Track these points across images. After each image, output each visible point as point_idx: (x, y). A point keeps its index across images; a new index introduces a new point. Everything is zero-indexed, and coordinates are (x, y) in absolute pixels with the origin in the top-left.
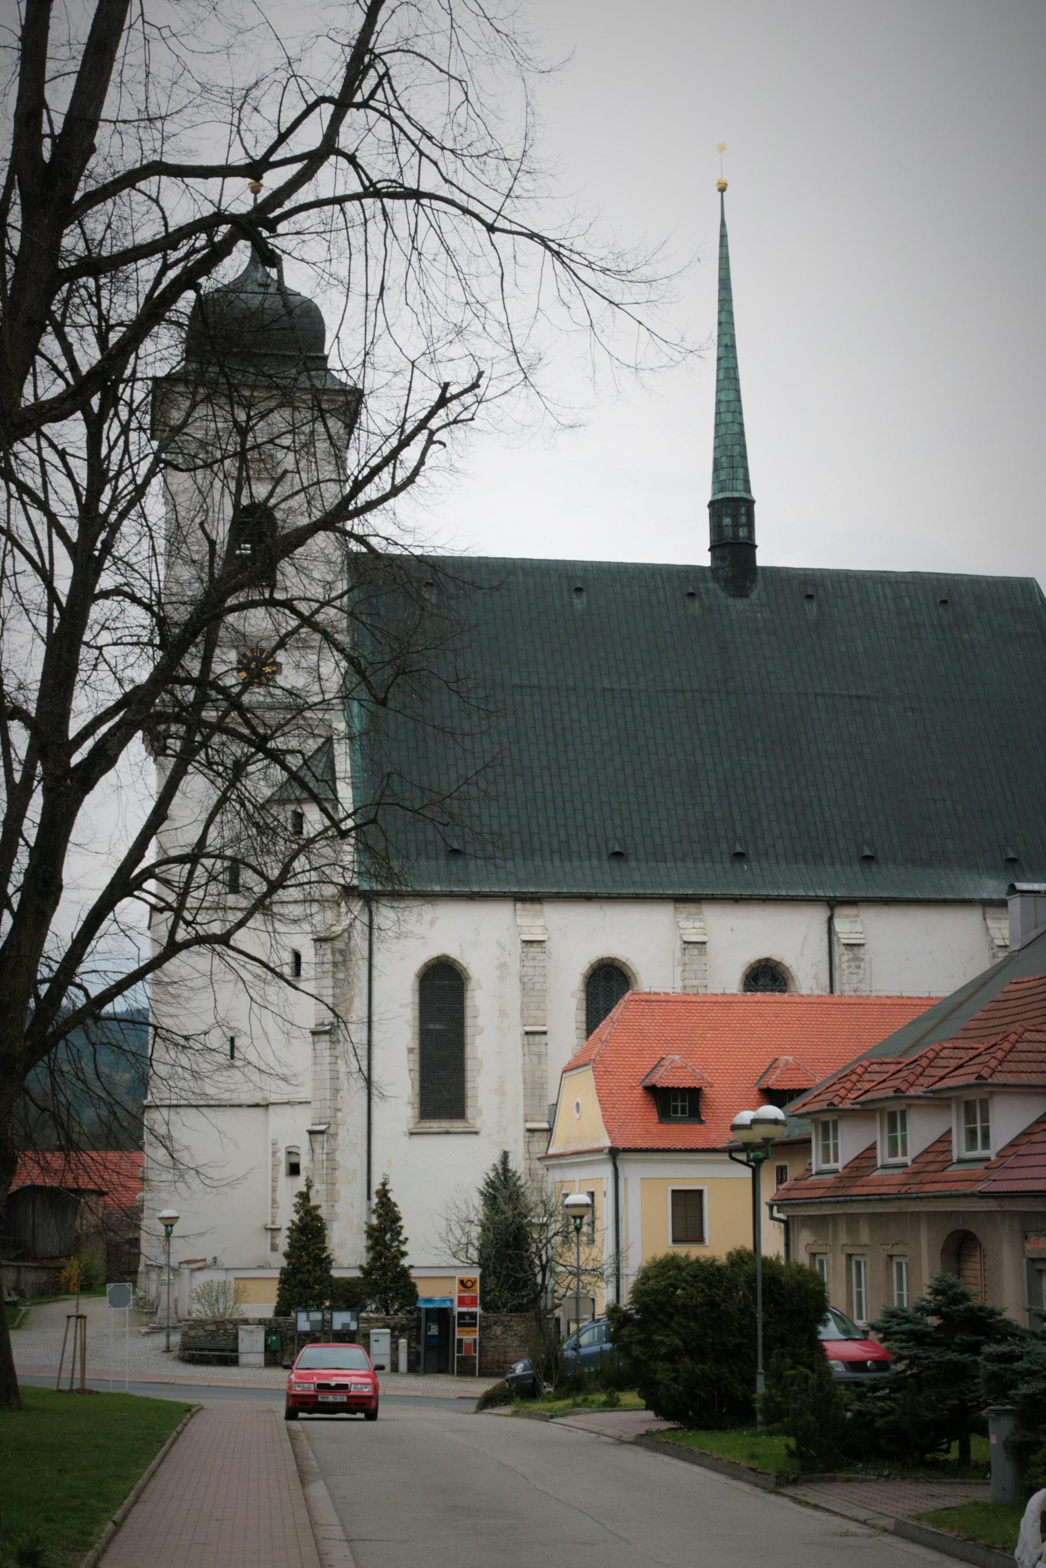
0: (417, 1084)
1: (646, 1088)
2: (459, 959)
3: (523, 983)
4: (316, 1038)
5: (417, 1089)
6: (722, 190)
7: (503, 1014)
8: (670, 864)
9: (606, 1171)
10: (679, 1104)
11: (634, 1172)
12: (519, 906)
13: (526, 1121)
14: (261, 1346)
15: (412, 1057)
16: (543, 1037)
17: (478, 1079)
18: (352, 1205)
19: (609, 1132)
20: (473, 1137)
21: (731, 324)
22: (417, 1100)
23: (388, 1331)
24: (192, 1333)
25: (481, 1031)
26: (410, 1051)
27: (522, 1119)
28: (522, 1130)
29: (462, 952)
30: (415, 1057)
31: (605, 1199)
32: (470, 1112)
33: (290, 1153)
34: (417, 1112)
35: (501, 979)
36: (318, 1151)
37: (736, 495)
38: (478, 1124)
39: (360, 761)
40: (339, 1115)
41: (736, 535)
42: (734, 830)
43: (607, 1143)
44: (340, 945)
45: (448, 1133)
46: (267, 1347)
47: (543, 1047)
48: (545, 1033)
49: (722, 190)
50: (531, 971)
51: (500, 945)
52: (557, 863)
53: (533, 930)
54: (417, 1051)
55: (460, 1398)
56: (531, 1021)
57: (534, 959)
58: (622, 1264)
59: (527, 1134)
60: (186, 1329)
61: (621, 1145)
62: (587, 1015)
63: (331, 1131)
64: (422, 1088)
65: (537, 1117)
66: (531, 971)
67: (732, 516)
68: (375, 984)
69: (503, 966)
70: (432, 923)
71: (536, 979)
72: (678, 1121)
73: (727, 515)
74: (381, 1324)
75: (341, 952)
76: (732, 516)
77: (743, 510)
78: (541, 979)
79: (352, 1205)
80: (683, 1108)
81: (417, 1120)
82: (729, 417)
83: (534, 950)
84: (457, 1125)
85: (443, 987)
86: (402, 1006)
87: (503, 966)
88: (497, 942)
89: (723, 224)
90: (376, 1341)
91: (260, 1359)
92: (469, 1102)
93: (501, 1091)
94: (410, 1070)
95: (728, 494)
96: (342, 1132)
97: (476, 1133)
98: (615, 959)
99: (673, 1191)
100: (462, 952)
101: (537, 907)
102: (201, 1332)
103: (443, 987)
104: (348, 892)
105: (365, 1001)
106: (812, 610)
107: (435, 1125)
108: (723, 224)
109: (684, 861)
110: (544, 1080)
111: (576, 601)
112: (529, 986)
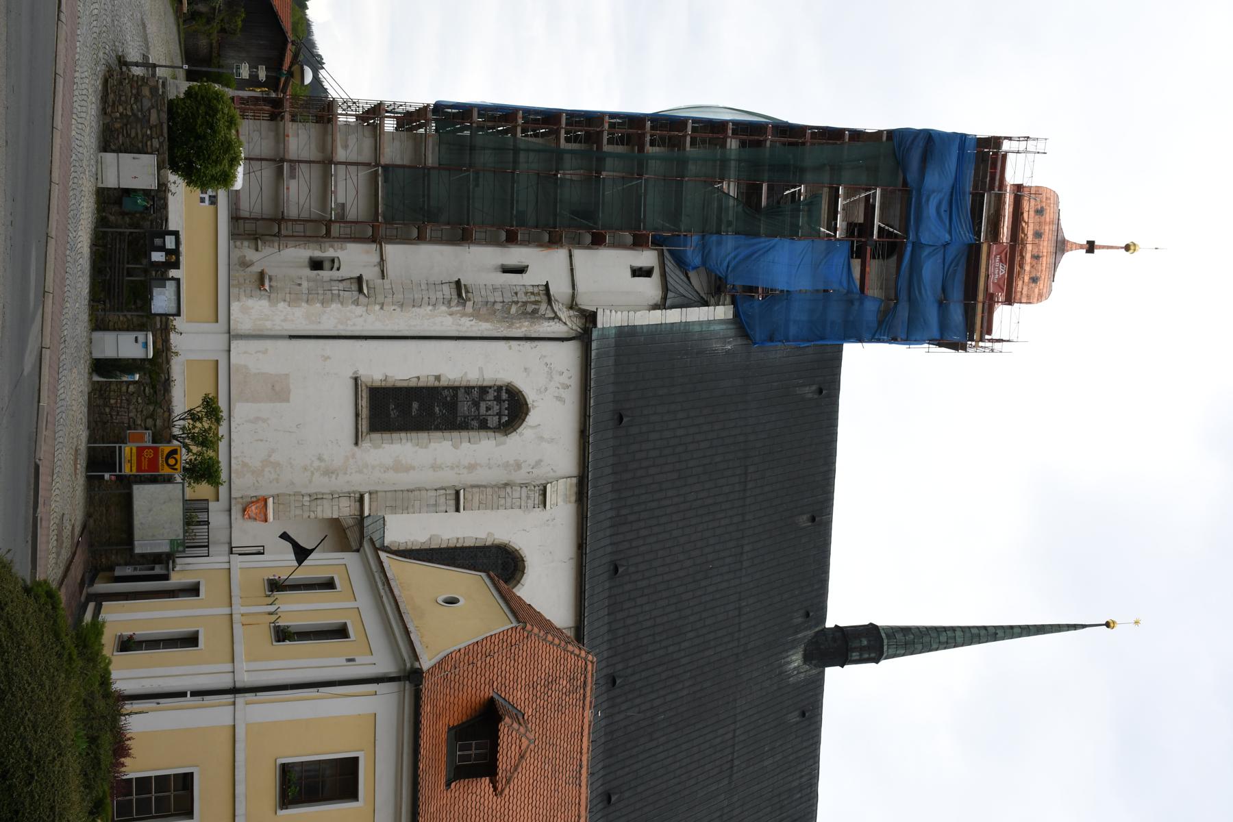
0: (405, 384)
1: (491, 702)
2: (524, 424)
3: (506, 485)
4: (453, 286)
5: (399, 384)
6: (1107, 625)
7: (472, 467)
8: (606, 619)
9: (383, 663)
10: (473, 752)
11: (383, 704)
12: (574, 480)
13: (370, 493)
14: (127, 184)
15: (432, 379)
16: (453, 508)
17: (409, 444)
18: (285, 320)
19: (440, 663)
20: (352, 440)
21: (1012, 637)
22: (389, 384)
23: (151, 355)
24: (146, 91)
25: (456, 447)
26: (438, 378)
27: (372, 489)
28: (362, 489)
29: (531, 427)
30: (431, 382)
31: (342, 661)
32: (376, 436)
33: (333, 261)
34: (377, 384)
35: (506, 465)
36: (341, 286)
37: (885, 648)
38: (366, 444)
39: (697, 328)
40: (377, 307)
41: (854, 650)
42: (632, 675)
43: (426, 663)
44: (543, 307)
45: (357, 415)
46: (127, 192)
47: (444, 508)
48: (457, 510)
49: (1107, 625)
50: (516, 495)
51: (539, 462)
52: (610, 514)
53: (554, 496)
54: (437, 384)
55: (37, 468)
56: (469, 496)
57: (528, 497)
58: (250, 697)
59: (357, 495)
60: (152, 83)
61: (426, 685)
62: (470, 548)
63: (361, 297)
64: (400, 389)
65: (374, 504)
66: (516, 495)
67: (869, 644)
68: (502, 344)
69: (518, 466)
70: (559, 398)
71: (509, 500)
72: (451, 753)
73: (869, 641)
74: (159, 346)
75: (535, 312)
76: (869, 644)
77: (873, 655)
78: (508, 504)
79: (285, 320)
80: (468, 757)
81: (369, 384)
82: (943, 639)
83: (537, 497)
84: (364, 425)
85: (508, 409)
86: (481, 369)
87: (518, 466)
88: (541, 461)
89: (1084, 626)
90: (136, 340)
91: (111, 182)
92: (386, 436)
93: (398, 467)
94: (418, 378)
95: (885, 641)
96: (359, 310)
97: (356, 444)
98: (523, 573)
99: (356, 760)
100: (531, 427)
101: (573, 498)
102: (147, 104)
103: (508, 409)
104: (590, 318)
105: (486, 334)
106: (794, 717)
107: (364, 403)
108: (1084, 626)
109: (609, 631)
110: (411, 510)
111: (805, 517)
112: (502, 494)
